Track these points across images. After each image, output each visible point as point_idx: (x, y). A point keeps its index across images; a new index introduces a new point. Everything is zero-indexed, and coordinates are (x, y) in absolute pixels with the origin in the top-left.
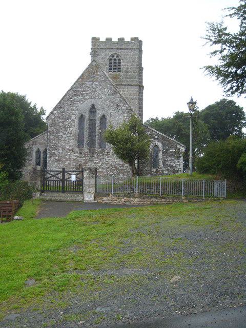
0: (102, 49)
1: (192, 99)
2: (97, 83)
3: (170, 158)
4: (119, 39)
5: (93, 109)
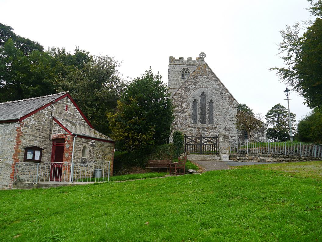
0: (177, 64)
1: (287, 88)
2: (206, 77)
3: (256, 133)
4: (188, 59)
5: (203, 95)
